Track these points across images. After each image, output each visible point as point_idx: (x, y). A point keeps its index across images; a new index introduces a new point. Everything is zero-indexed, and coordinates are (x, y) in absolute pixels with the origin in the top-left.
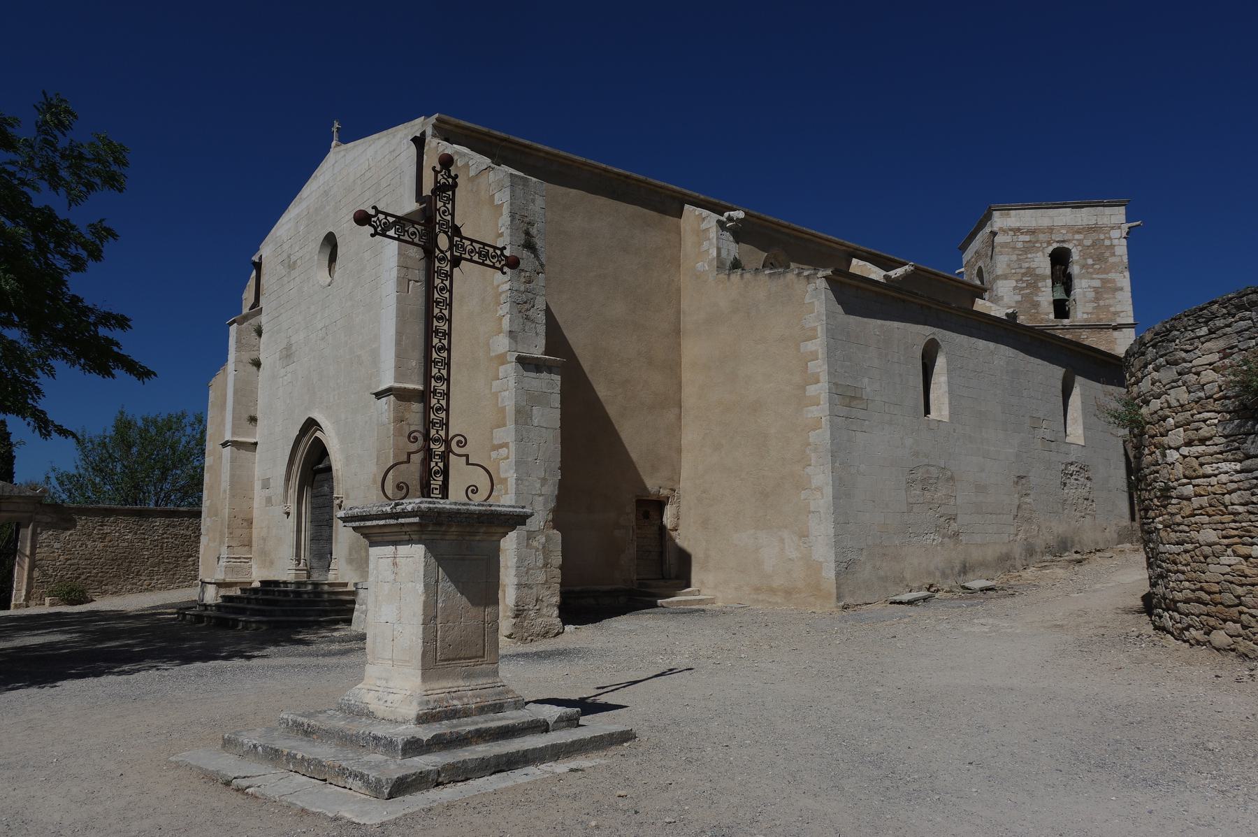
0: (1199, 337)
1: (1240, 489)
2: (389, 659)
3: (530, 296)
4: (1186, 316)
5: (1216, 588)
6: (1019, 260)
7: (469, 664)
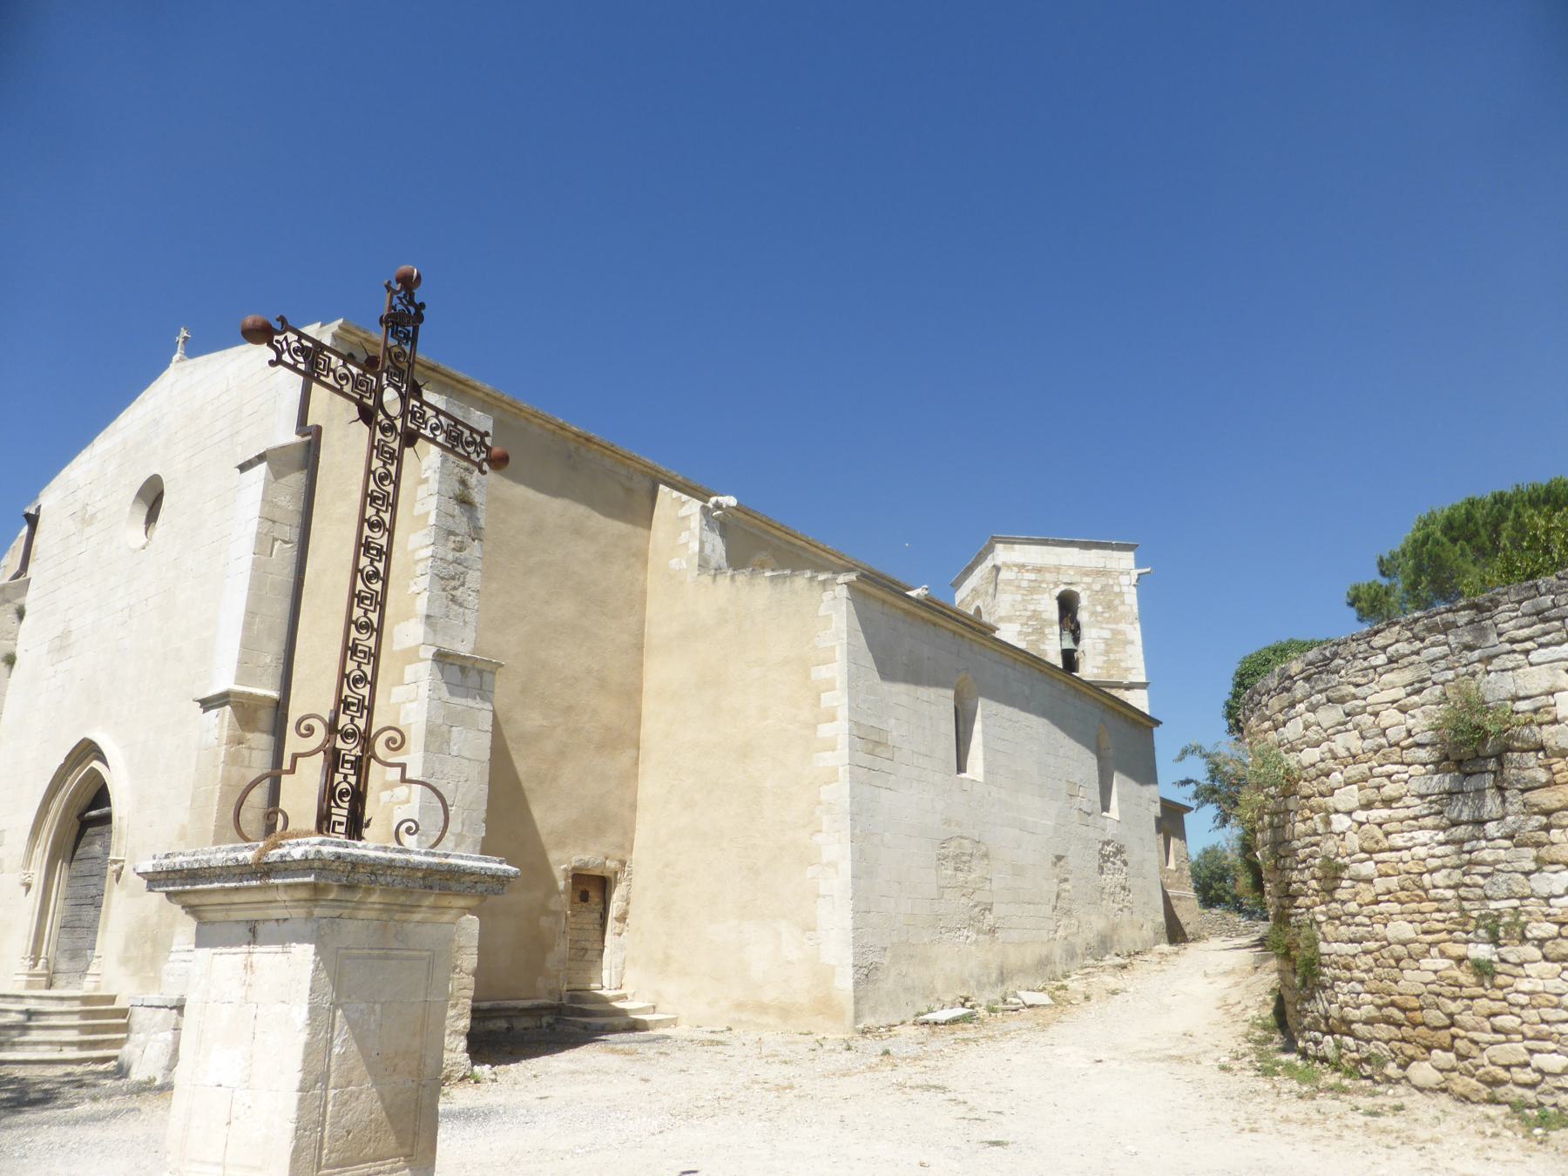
0: (1375, 668)
1: (1444, 867)
2: (218, 1164)
3: (461, 569)
4: (1353, 640)
5: (1415, 1003)
6: (1023, 600)
7: (382, 1168)
